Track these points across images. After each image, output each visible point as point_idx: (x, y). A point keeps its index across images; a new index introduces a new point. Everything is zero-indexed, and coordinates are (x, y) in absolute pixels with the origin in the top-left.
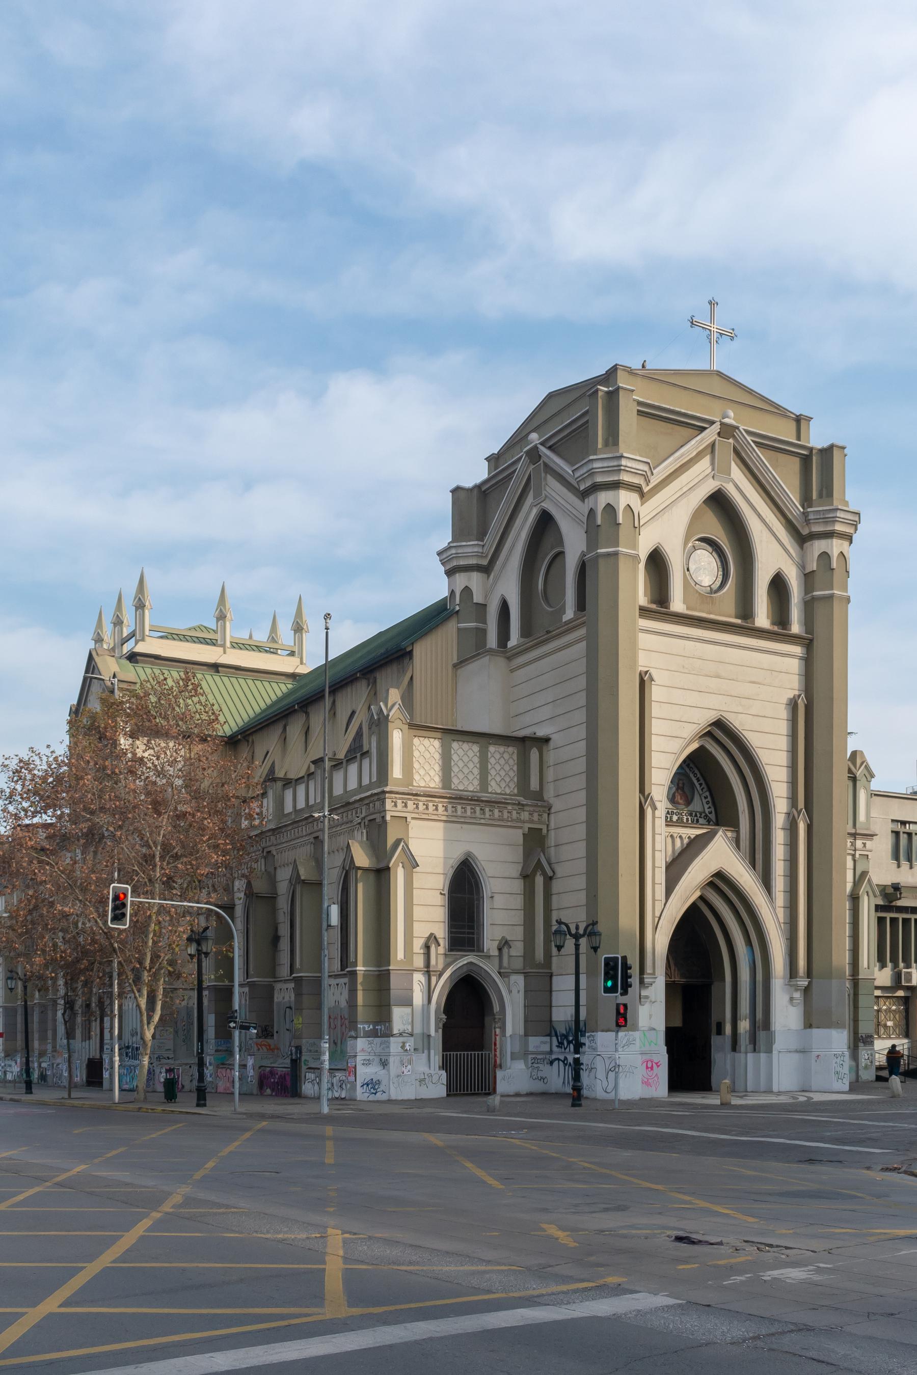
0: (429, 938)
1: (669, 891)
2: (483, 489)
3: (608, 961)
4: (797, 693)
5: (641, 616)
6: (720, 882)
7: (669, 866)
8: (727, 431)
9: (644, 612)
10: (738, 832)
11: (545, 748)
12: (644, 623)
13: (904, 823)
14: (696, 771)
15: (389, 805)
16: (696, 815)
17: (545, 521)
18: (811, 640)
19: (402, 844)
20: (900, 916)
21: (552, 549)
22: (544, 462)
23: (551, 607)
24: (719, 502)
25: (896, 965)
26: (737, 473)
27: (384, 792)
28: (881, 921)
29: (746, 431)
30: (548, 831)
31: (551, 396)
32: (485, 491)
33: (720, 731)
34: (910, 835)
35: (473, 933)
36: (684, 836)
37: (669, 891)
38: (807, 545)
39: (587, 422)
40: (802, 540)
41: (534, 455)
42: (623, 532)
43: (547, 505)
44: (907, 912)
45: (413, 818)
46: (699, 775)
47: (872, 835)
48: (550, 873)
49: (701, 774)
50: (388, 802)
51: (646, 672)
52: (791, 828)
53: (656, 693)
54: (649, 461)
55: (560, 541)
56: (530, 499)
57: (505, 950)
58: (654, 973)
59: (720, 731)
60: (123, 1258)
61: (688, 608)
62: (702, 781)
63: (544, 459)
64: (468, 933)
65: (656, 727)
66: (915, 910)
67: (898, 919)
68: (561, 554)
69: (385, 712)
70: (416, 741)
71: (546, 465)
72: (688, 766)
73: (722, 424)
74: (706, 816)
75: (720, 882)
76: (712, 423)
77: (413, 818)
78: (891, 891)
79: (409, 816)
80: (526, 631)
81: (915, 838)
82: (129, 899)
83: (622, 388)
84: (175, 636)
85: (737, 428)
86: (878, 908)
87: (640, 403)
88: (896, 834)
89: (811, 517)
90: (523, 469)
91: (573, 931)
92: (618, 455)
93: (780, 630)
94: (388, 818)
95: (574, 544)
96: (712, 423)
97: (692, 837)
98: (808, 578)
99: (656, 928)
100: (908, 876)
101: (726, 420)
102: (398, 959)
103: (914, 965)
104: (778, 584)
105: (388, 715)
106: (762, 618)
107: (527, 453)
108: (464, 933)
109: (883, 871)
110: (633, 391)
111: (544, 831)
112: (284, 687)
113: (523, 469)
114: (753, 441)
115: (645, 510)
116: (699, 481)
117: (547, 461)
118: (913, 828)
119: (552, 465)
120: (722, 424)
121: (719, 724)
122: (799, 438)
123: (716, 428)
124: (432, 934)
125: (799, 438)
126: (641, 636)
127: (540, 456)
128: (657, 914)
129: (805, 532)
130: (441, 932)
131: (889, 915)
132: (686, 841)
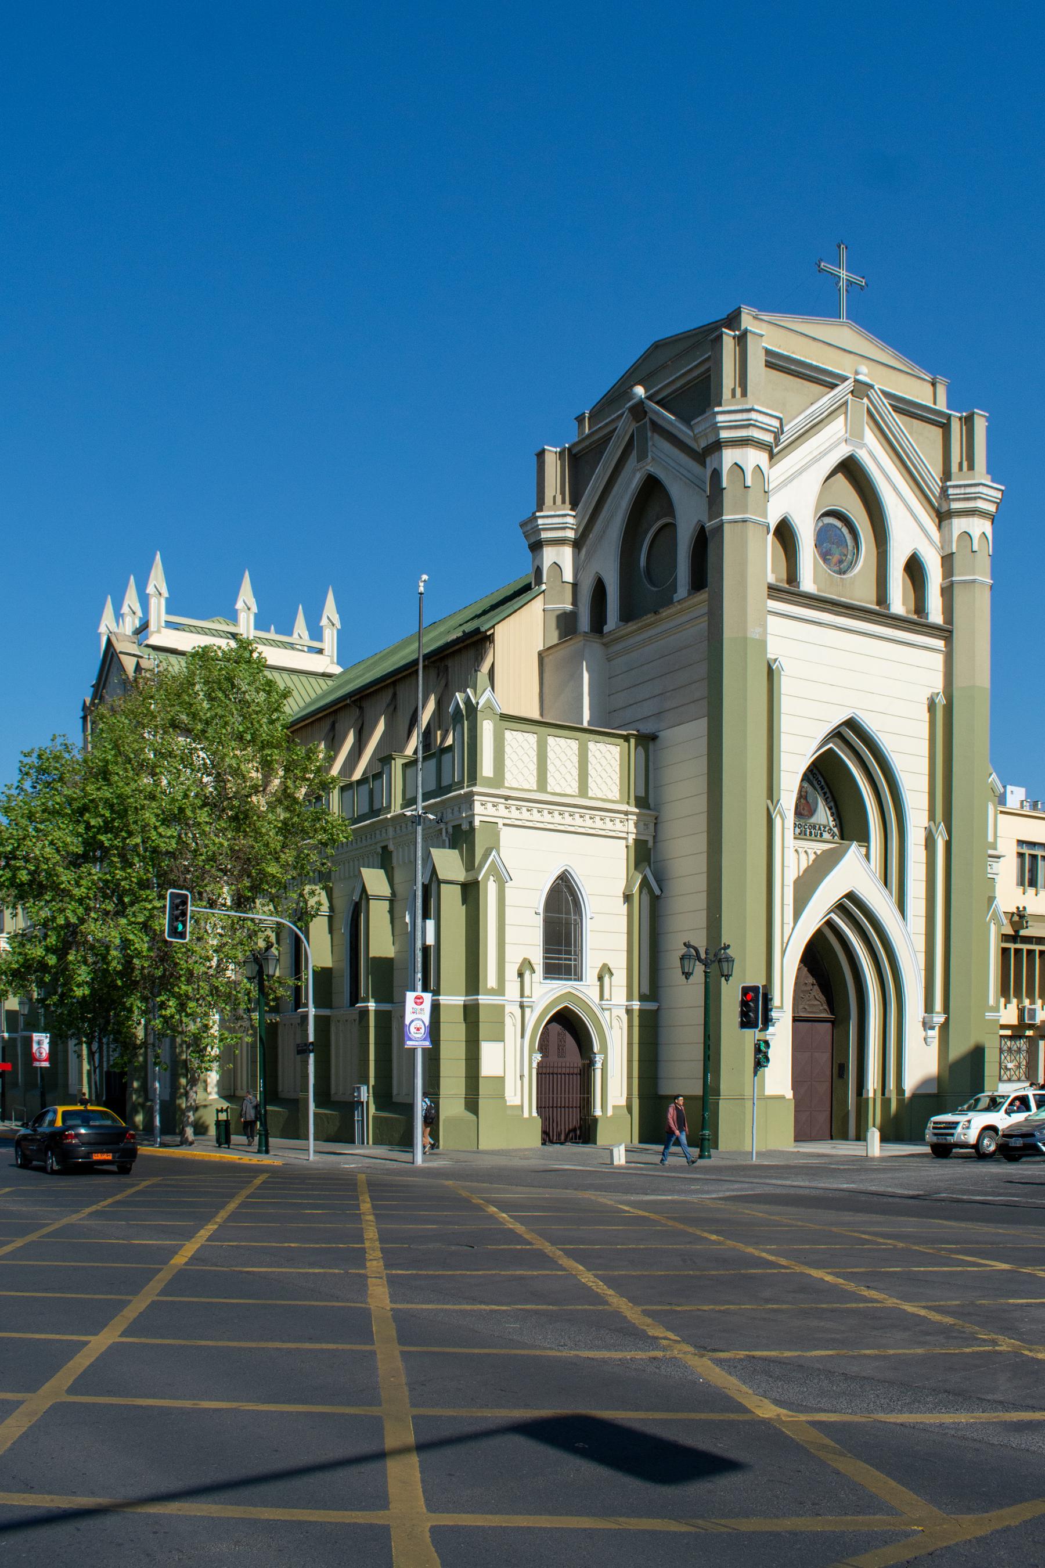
0: (522, 965)
1: (797, 915)
2: (574, 452)
3: (746, 990)
4: (937, 691)
5: (770, 597)
6: (851, 906)
7: (797, 882)
8: (861, 389)
9: (774, 592)
10: (868, 848)
11: (651, 746)
12: (773, 605)
13: (1032, 844)
14: (820, 778)
15: (478, 808)
16: (820, 829)
17: (652, 487)
18: (951, 632)
19: (494, 853)
20: (1025, 947)
21: (658, 519)
22: (651, 419)
23: (654, 585)
24: (850, 469)
25: (1020, 1001)
26: (870, 438)
27: (472, 792)
28: (1005, 951)
29: (883, 392)
30: (655, 842)
31: (657, 346)
32: (575, 455)
33: (851, 734)
34: (1034, 857)
35: (570, 960)
36: (809, 851)
37: (797, 915)
38: (945, 523)
39: (708, 370)
40: (943, 516)
41: (639, 410)
42: (753, 495)
43: (651, 468)
44: (1031, 943)
45: (504, 825)
46: (823, 783)
47: (999, 857)
48: (657, 892)
49: (825, 782)
50: (477, 805)
51: (776, 660)
52: (930, 843)
53: (786, 685)
54: (781, 416)
55: (669, 508)
56: (632, 460)
57: (606, 979)
58: (782, 1007)
59: (851, 734)
60: (122, 1305)
61: (818, 590)
62: (826, 790)
63: (650, 415)
64: (566, 959)
65: (786, 724)
66: (1039, 940)
67: (1009, 949)
68: (671, 528)
69: (474, 702)
70: (508, 734)
71: (653, 423)
72: (813, 774)
73: (856, 381)
74: (830, 829)
75: (851, 906)
76: (845, 379)
77: (504, 825)
78: (1016, 918)
79: (500, 822)
80: (627, 615)
81: (1040, 863)
82: (189, 908)
83: (751, 332)
84: (192, 629)
85: (872, 387)
86: (1006, 938)
87: (768, 352)
88: (1021, 855)
89: (951, 491)
90: (626, 427)
91: (703, 956)
92: (748, 407)
93: (916, 622)
94: (477, 823)
95: (688, 516)
96: (845, 379)
97: (819, 852)
98: (948, 561)
99: (783, 952)
100: (1043, 902)
101: (860, 377)
102: (489, 986)
103: (1039, 1002)
104: (914, 568)
105: (478, 703)
106: (899, 604)
107: (632, 409)
108: (559, 959)
109: (1009, 895)
110: (762, 336)
111: (651, 844)
112: (325, 685)
113: (626, 427)
114: (890, 405)
115: (776, 474)
116: (831, 444)
117: (655, 418)
118: (1039, 853)
119: (660, 422)
120: (856, 381)
121: (851, 723)
122: (935, 404)
123: (848, 385)
124: (525, 959)
125: (935, 404)
126: (770, 619)
127: (646, 412)
128: (785, 941)
129: (944, 509)
130: (537, 958)
131: (1012, 946)
132: (812, 857)
